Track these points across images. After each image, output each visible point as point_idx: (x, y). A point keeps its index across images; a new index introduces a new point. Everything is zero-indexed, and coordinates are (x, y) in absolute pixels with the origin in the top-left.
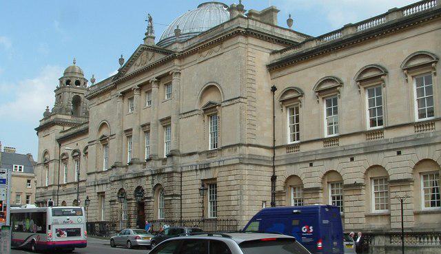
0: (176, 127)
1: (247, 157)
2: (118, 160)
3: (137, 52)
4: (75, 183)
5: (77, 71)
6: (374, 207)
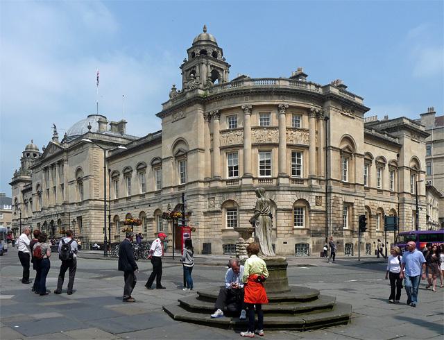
4: (156, 193)
5: (34, 147)
6: (226, 225)
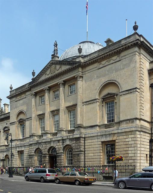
0: (81, 110)
1: (140, 126)
2: (81, 123)
3: (50, 64)
